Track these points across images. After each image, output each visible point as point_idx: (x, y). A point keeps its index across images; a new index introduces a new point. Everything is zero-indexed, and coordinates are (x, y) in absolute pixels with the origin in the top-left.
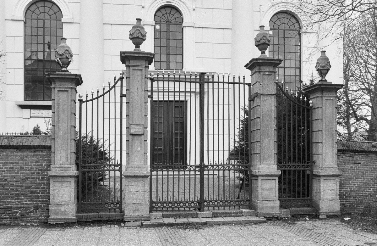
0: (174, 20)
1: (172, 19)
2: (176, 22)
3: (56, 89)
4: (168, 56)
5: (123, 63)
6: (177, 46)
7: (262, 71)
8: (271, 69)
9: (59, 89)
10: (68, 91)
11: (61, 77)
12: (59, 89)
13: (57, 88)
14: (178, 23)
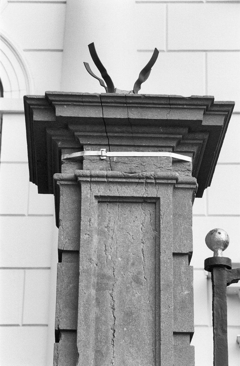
3: (85, 188)
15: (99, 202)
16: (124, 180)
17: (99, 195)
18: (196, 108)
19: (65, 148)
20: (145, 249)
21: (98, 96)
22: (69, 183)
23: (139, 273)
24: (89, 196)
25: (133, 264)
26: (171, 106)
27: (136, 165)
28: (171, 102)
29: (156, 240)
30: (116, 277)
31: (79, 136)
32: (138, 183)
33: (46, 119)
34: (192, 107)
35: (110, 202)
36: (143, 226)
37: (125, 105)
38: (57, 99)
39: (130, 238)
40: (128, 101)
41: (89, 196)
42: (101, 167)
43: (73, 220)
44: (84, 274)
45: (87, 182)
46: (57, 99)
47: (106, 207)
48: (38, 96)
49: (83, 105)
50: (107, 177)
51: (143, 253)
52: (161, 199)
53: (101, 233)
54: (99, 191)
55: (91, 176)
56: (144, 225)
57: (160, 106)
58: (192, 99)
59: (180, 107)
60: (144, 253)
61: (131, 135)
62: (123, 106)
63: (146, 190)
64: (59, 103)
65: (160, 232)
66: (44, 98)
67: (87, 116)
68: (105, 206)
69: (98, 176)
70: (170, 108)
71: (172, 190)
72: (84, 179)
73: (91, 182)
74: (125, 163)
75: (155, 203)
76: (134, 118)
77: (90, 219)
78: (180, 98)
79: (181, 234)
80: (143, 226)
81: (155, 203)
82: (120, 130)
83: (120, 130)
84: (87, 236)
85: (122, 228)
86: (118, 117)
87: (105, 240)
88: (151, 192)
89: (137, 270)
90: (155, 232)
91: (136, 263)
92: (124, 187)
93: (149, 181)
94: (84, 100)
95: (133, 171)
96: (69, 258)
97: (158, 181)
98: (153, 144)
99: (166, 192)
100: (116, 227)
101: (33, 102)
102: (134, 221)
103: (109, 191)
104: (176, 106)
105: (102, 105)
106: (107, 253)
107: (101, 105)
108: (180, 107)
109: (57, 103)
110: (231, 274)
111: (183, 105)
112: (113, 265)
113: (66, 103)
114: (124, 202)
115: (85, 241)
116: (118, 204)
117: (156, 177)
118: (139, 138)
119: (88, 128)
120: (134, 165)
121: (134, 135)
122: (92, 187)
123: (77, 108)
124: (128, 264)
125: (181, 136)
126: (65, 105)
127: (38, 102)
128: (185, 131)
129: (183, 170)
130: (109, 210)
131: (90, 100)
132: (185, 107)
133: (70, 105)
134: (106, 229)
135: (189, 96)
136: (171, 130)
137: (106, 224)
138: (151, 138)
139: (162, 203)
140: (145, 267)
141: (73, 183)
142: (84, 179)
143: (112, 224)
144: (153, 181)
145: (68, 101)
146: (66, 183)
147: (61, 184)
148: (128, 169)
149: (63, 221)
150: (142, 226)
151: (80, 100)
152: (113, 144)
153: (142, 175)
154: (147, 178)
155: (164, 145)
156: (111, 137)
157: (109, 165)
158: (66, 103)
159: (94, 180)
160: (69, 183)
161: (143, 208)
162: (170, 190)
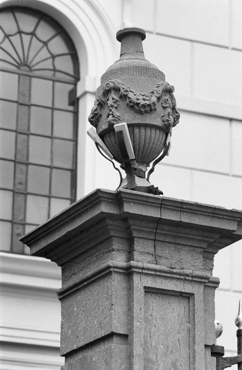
0: (48, 64)
1: (39, 57)
2: (55, 70)
3: (136, 279)
4: (20, 198)
5: (157, 188)
6: (56, 164)
7: (144, 272)
8: (190, 263)
9: (150, 282)
10: (188, 297)
11: (173, 217)
12: (150, 282)
13: (144, 272)
14: (59, 76)
15: (145, 292)
16: (168, 275)
17: (147, 286)
18: (233, 220)
19: (117, 237)
20: (180, 339)
21: (161, 199)
22: (121, 271)
23: (177, 360)
24: (139, 286)
25: (172, 352)
26: (215, 215)
27: (176, 261)
28: (216, 212)
29: (189, 332)
30: (159, 362)
31: (134, 229)
32: (178, 279)
33: (112, 212)
34: (230, 218)
35: (153, 293)
36: (179, 317)
37: (180, 209)
38: (127, 196)
39: (169, 327)
40: (183, 206)
41: (139, 286)
42: (148, 259)
43: (123, 306)
44: (137, 358)
45: (138, 273)
46: (127, 196)
47: (150, 297)
48: (110, 190)
49: (146, 205)
50: (155, 270)
51: (179, 343)
52: (195, 295)
53: (147, 320)
54: (147, 283)
55: (143, 268)
56: (180, 317)
57: (206, 214)
58: (232, 212)
59: (221, 216)
60: (180, 343)
61: (175, 234)
62: (177, 210)
63: (183, 285)
64: (128, 200)
65: (194, 325)
66: (115, 193)
67: (148, 215)
68: (149, 295)
69: (149, 269)
70: (213, 216)
71: (203, 288)
72: (137, 270)
73: (142, 273)
74: (167, 258)
75: (189, 298)
76: (185, 221)
77: (141, 307)
78: (224, 210)
79: (207, 328)
80: (179, 317)
81: (189, 298)
82: (168, 229)
83: (168, 229)
84: (139, 323)
85: (163, 318)
86: (173, 219)
87: (150, 327)
88: (187, 288)
89: (175, 357)
90: (189, 324)
91: (174, 351)
92: (167, 281)
93: (187, 278)
94: (148, 200)
95: (173, 267)
96: (119, 340)
97: (194, 279)
98: (189, 244)
99: (199, 289)
100: (158, 317)
101: (105, 196)
102: (172, 313)
103: (155, 283)
104: (218, 216)
105: (161, 206)
106: (152, 340)
107: (160, 206)
108: (221, 216)
109: (126, 200)
110: (225, 361)
111: (224, 215)
112: (156, 351)
113: (133, 201)
114: (164, 294)
115: (137, 328)
116: (159, 295)
117: (194, 275)
118: (180, 237)
119: (144, 224)
120: (174, 261)
121: (178, 234)
122: (142, 278)
123: (141, 206)
124: (168, 351)
125: (213, 240)
126: (131, 202)
127: (109, 196)
128: (218, 236)
129: (207, 268)
130: (152, 300)
131: (154, 201)
132: (225, 217)
133: (136, 203)
134: (150, 317)
135: (231, 209)
136: (208, 234)
137: (150, 313)
138: (190, 239)
139: (196, 298)
140: (181, 355)
141: (125, 271)
142: (137, 270)
143: (154, 314)
144: (190, 279)
145: (136, 200)
146: (118, 270)
147: (114, 271)
148: (169, 264)
149: (115, 305)
150: (178, 317)
151: (146, 200)
152: (158, 239)
153: (183, 272)
154: (187, 275)
155: (198, 246)
156: (159, 233)
157: (155, 259)
158: (133, 201)
159: (145, 272)
160: (121, 271)
161: (179, 301)
162: (202, 287)
